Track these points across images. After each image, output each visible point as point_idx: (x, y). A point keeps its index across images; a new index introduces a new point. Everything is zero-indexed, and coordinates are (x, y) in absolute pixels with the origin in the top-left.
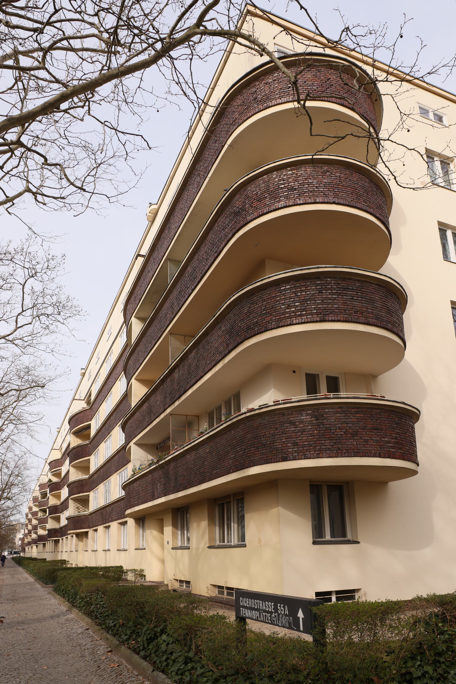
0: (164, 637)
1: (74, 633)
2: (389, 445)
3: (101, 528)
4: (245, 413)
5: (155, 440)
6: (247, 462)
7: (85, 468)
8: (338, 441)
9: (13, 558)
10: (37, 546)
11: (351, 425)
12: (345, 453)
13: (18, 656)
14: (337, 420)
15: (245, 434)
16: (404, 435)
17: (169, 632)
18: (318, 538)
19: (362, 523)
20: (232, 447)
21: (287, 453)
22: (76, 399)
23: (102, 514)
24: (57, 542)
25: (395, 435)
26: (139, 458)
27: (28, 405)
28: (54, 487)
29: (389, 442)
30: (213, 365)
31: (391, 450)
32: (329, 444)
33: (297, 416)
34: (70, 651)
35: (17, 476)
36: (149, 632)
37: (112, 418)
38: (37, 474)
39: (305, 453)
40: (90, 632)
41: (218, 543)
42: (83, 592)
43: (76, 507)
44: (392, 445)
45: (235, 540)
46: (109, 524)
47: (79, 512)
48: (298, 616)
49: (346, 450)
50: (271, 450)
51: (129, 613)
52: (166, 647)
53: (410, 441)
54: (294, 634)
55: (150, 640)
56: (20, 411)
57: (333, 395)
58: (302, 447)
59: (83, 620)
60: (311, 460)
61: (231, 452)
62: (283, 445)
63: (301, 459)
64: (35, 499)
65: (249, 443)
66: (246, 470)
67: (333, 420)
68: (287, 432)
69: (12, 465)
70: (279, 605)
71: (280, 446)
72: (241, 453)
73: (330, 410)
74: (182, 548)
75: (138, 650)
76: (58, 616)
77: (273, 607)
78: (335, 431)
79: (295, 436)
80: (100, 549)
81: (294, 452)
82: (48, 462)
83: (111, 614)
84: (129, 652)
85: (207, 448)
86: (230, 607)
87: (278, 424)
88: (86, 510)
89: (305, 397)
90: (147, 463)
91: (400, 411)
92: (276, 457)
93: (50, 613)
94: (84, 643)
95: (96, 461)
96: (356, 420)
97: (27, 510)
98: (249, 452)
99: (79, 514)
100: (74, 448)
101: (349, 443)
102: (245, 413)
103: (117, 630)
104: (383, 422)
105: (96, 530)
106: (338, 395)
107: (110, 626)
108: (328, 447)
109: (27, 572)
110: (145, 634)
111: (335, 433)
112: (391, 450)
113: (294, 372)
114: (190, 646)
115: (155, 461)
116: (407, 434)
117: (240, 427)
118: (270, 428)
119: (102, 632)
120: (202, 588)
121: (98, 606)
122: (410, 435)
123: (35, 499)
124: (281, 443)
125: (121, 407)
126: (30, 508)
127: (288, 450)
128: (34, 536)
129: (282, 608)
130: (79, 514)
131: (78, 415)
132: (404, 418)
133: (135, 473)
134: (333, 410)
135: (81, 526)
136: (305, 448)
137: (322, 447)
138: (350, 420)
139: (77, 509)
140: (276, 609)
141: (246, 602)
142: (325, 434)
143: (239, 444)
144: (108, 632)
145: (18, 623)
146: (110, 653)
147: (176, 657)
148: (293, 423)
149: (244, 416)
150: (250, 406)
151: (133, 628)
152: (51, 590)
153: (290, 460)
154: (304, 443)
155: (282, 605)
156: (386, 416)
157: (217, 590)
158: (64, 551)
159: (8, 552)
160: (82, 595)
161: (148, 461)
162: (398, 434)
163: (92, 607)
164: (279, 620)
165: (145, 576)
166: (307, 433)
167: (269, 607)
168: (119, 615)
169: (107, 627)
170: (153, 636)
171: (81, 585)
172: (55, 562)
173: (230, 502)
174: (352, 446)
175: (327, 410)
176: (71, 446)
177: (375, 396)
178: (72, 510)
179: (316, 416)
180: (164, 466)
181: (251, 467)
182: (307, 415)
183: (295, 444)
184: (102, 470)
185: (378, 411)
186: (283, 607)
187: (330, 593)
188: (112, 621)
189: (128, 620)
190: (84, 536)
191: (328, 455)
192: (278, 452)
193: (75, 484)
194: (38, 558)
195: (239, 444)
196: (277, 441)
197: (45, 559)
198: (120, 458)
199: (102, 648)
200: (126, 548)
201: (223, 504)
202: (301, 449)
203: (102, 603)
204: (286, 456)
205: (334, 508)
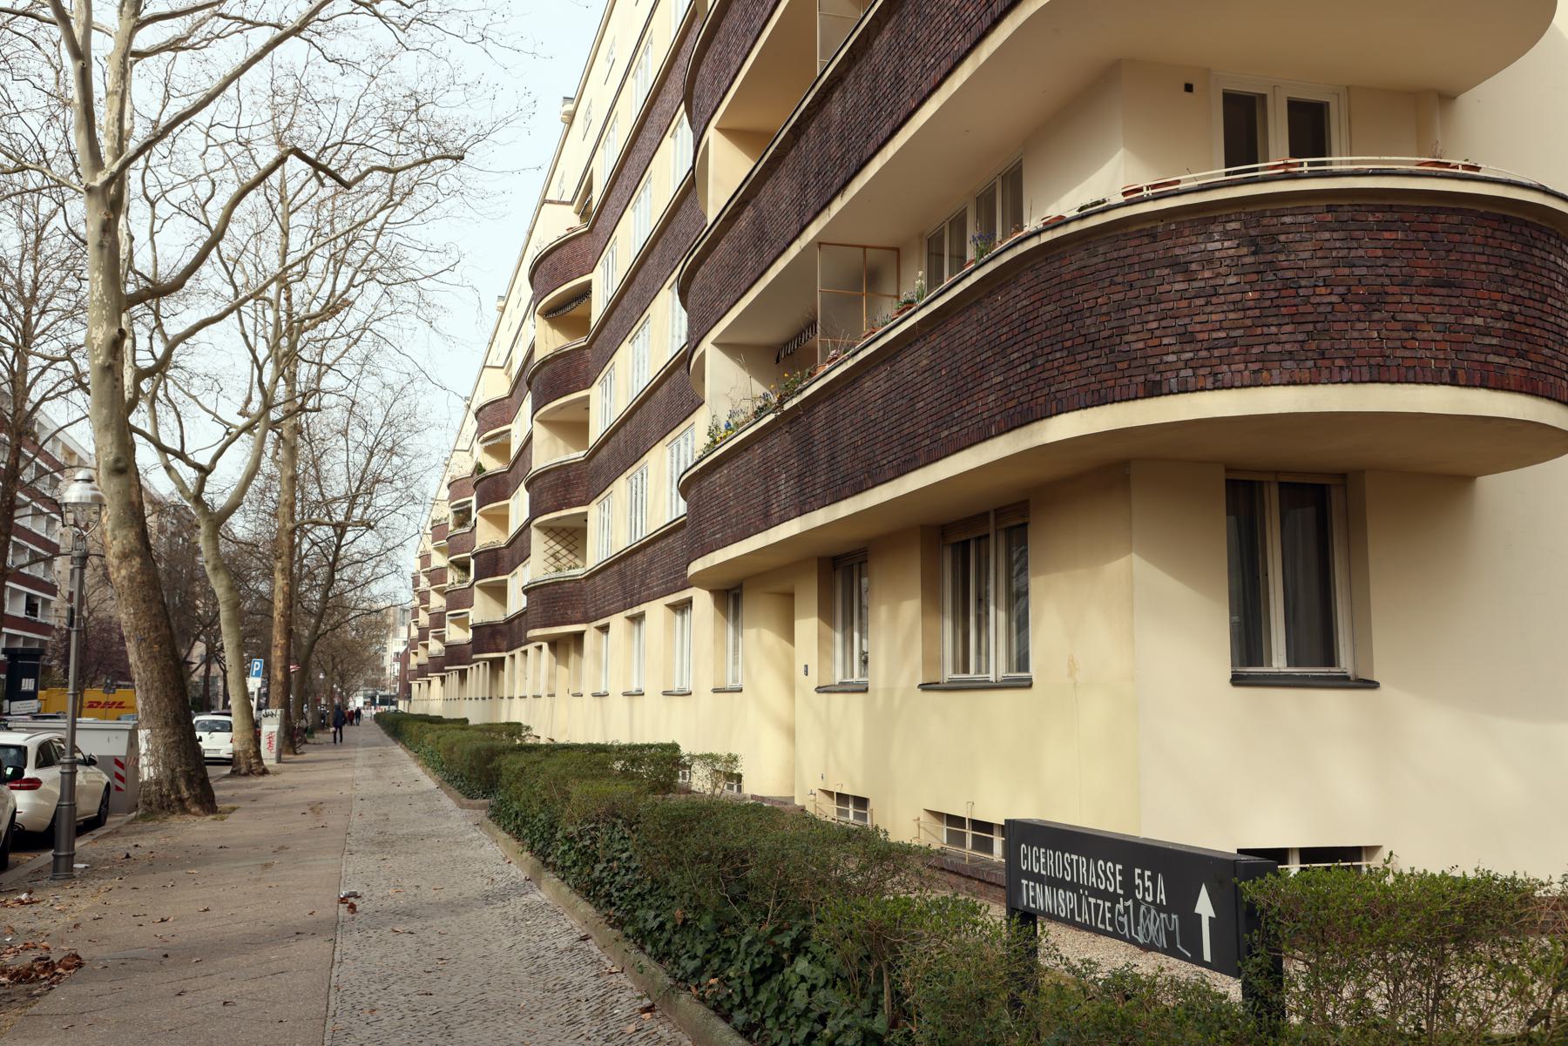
0: (802, 965)
1: (547, 949)
2: (1487, 340)
3: (618, 622)
4: (1038, 233)
5: (772, 332)
6: (1041, 400)
7: (574, 427)
8: (1319, 326)
9: (378, 718)
10: (443, 679)
11: (1364, 271)
12: (1341, 368)
13: (399, 1015)
14: (1319, 254)
15: (1037, 304)
16: (1538, 305)
17: (815, 949)
18: (1248, 663)
19: (1392, 618)
20: (997, 350)
21: (1162, 368)
22: (551, 202)
23: (622, 574)
24: (497, 665)
25: (1505, 307)
26: (730, 391)
27: (417, 220)
28: (491, 488)
29: (1486, 331)
30: (944, 70)
31: (1491, 358)
32: (1293, 338)
33: (1194, 239)
34: (537, 1005)
35: (391, 450)
36: (759, 946)
37: (650, 261)
38: (445, 449)
39: (1216, 369)
40: (593, 946)
41: (948, 674)
42: (571, 820)
43: (551, 552)
44: (1494, 341)
45: (998, 668)
46: (642, 607)
47: (559, 570)
48: (1197, 910)
49: (1346, 358)
50: (1112, 357)
51: (702, 885)
52: (806, 1000)
53: (1555, 329)
54: (1183, 970)
55: (762, 975)
56: (397, 239)
57: (1310, 164)
58: (1208, 349)
59: (572, 908)
60: (1234, 392)
61: (995, 366)
62: (1150, 343)
63: (1203, 389)
64: (438, 529)
65: (1046, 334)
66: (1036, 426)
67: (1307, 255)
68: (1164, 297)
69: (377, 419)
70: (1138, 871)
71: (1141, 345)
72: (1023, 368)
73: (1300, 219)
74: (845, 688)
75: (727, 1006)
76: (504, 896)
77: (1119, 878)
78: (1310, 291)
79: (1186, 311)
80: (615, 689)
81: (1181, 365)
82: (475, 407)
83: (650, 891)
84: (701, 1011)
85: (922, 356)
86: (982, 887)
87: (1137, 268)
88: (578, 562)
89: (1219, 173)
90: (749, 407)
91: (1527, 218)
92: (1126, 381)
93: (479, 885)
94: (577, 981)
95: (607, 401)
96: (1379, 253)
97: (414, 565)
98: (1048, 366)
99: (558, 574)
100: (544, 362)
101: (1355, 335)
102: (1038, 233)
103: (669, 942)
104: (1468, 257)
105: (605, 629)
106: (1324, 163)
107: (649, 927)
108: (1288, 347)
109: (416, 759)
110: (747, 954)
111: (1313, 300)
112: (1491, 358)
113: (1189, 88)
114: (877, 995)
115: (774, 399)
116: (1550, 300)
117: (1023, 280)
118: (1112, 283)
119: (626, 946)
120: (903, 821)
121: (615, 864)
122: (1559, 304)
123: (438, 529)
124: (1142, 336)
125: (677, 226)
126: (425, 558)
127: (1166, 358)
128: (435, 647)
129: (1148, 884)
130: (558, 574)
131: (556, 254)
132: (1539, 245)
133: (715, 442)
134: (1309, 219)
135: (566, 611)
136: (1216, 353)
137: (1271, 348)
138: (1361, 252)
139: (552, 560)
140: (1129, 887)
141: (1038, 860)
142: (1280, 302)
143: (1020, 337)
144: (642, 949)
145: (395, 913)
146: (648, 1015)
147: (836, 1030)
148: (1180, 267)
149: (1033, 243)
150: (1053, 211)
151: (712, 937)
152: (482, 814)
153: (1171, 393)
154: (1215, 335)
155: (1148, 873)
156: (1479, 239)
157: (943, 830)
158: (517, 696)
159: (365, 696)
160: (571, 829)
161: (754, 399)
162: (1519, 301)
163: (599, 867)
164: (1137, 924)
165: (739, 777)
166: (1222, 299)
167: (1107, 878)
168: (672, 893)
169: (639, 931)
170: (769, 962)
171: (566, 797)
172: (490, 727)
173: (987, 536)
174: (1364, 344)
175: (1287, 220)
176: (539, 356)
177: (1447, 165)
178: (537, 567)
179: (1252, 241)
180: (799, 417)
181: (1051, 416)
182: (1227, 235)
183: (1186, 338)
184: (622, 432)
185: (1456, 219)
186: (1150, 878)
187: (1281, 855)
188: (653, 913)
189: (699, 908)
190: (572, 648)
191: (1286, 377)
192: (1134, 364)
193: (547, 479)
194: (445, 717)
195: (1020, 337)
196: (1132, 329)
197: (466, 721)
198: (675, 392)
199: (627, 999)
200: (687, 687)
201: (966, 543)
202: (1204, 354)
203: (624, 855)
204: (1158, 377)
205: (1302, 557)
